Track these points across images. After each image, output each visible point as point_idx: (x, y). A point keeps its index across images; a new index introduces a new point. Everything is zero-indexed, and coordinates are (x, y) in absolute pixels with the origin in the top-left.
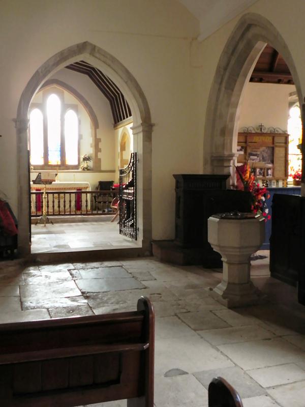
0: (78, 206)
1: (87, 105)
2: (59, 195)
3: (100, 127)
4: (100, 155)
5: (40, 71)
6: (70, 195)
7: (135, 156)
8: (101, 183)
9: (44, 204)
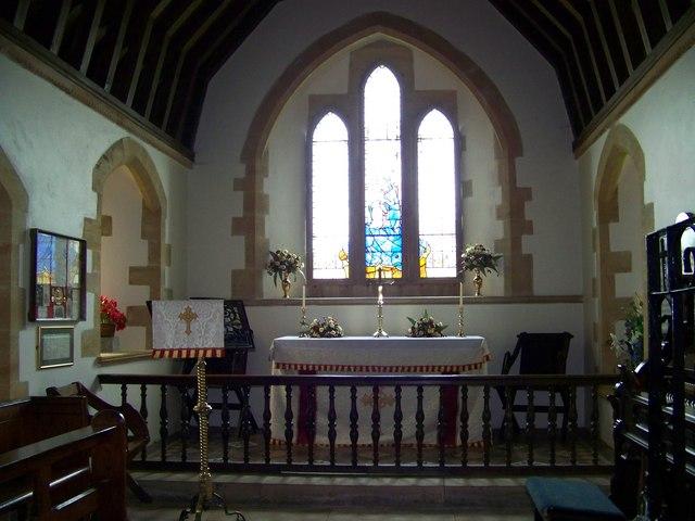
1: (480, 83)
2: (376, 391)
4: (528, 244)
8: (528, 342)
9: (322, 420)
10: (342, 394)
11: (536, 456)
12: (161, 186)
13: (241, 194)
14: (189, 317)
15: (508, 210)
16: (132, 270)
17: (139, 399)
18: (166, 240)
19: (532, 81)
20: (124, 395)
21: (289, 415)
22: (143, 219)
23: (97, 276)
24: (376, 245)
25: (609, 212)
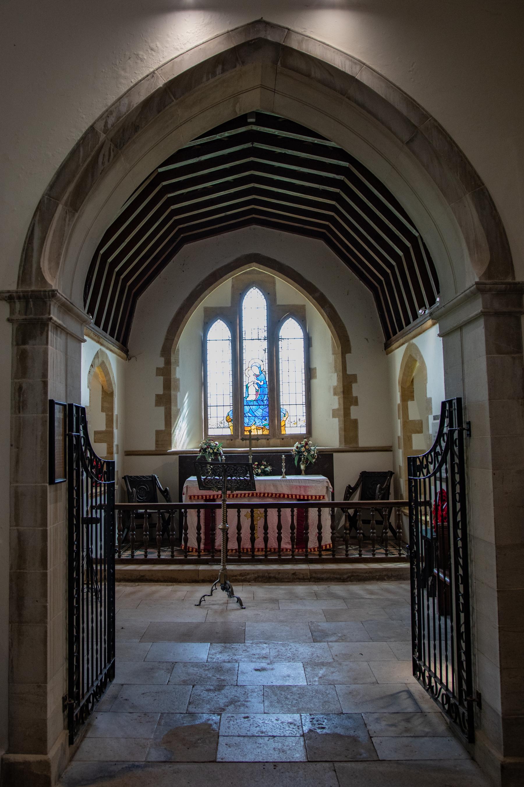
0: (300, 538)
3: (353, 349)
4: (355, 412)
5: (100, 127)
6: (279, 512)
7: (453, 410)
11: (363, 552)
12: (113, 377)
13: (161, 378)
15: (342, 390)
18: (116, 412)
19: (362, 324)
21: (199, 528)
24: (251, 412)
25: (408, 393)
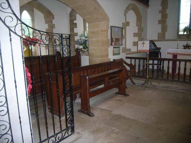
10: (183, 63)
14: (143, 43)
16: (134, 34)
17: (134, 62)
20: (131, 61)
22: (137, 22)
23: (125, 36)
